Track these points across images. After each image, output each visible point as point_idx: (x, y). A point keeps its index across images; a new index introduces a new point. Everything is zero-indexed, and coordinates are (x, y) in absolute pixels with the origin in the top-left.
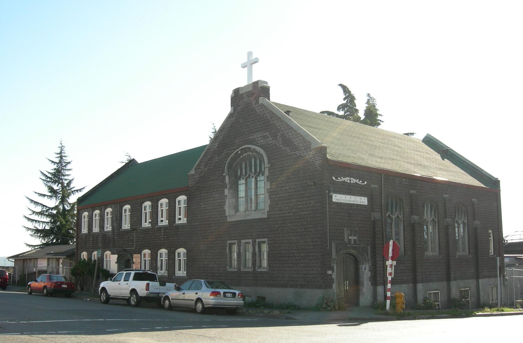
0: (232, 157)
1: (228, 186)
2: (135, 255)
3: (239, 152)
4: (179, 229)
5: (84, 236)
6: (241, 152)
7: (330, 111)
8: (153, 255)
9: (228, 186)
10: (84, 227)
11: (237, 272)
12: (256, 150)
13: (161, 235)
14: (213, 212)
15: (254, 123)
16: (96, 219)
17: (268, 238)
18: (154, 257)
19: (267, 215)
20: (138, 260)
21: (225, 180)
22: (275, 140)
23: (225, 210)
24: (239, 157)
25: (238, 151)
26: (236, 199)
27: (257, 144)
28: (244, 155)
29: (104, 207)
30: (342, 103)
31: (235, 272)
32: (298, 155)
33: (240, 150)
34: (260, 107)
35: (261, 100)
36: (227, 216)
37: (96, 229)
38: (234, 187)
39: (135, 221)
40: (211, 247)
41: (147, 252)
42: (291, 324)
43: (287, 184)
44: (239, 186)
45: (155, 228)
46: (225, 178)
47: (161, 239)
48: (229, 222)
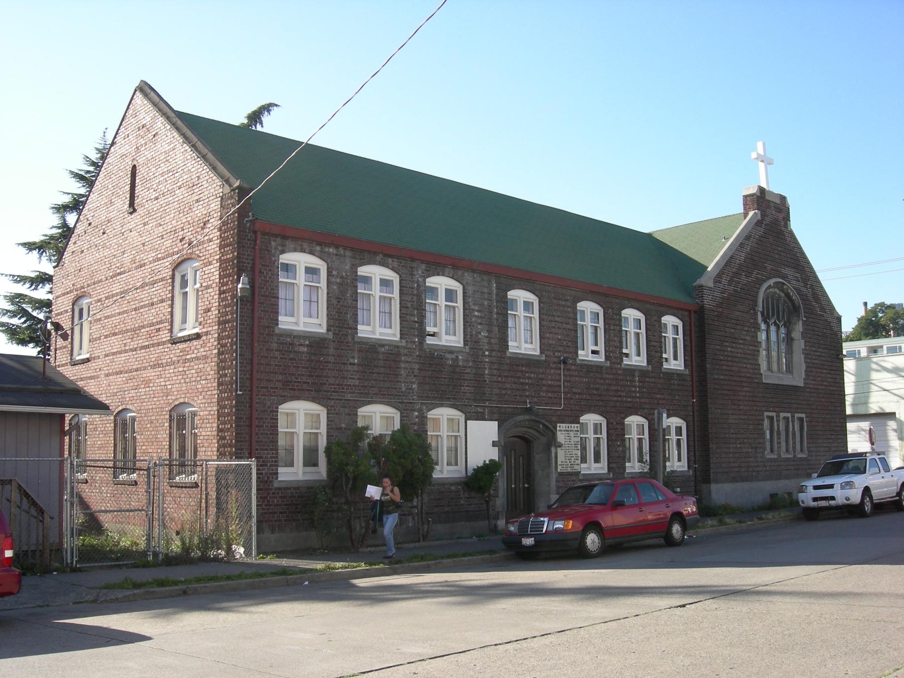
2: (561, 427)
4: (672, 379)
5: (307, 343)
7: (250, 112)
8: (617, 429)
11: (777, 459)
13: (635, 386)
14: (745, 363)
17: (806, 413)
18: (617, 434)
20: (572, 438)
29: (423, 266)
30: (259, 105)
31: (775, 458)
37: (636, 359)
39: (560, 340)
40: (744, 419)
41: (591, 419)
42: (218, 605)
45: (619, 369)
47: (634, 395)
48: (764, 383)
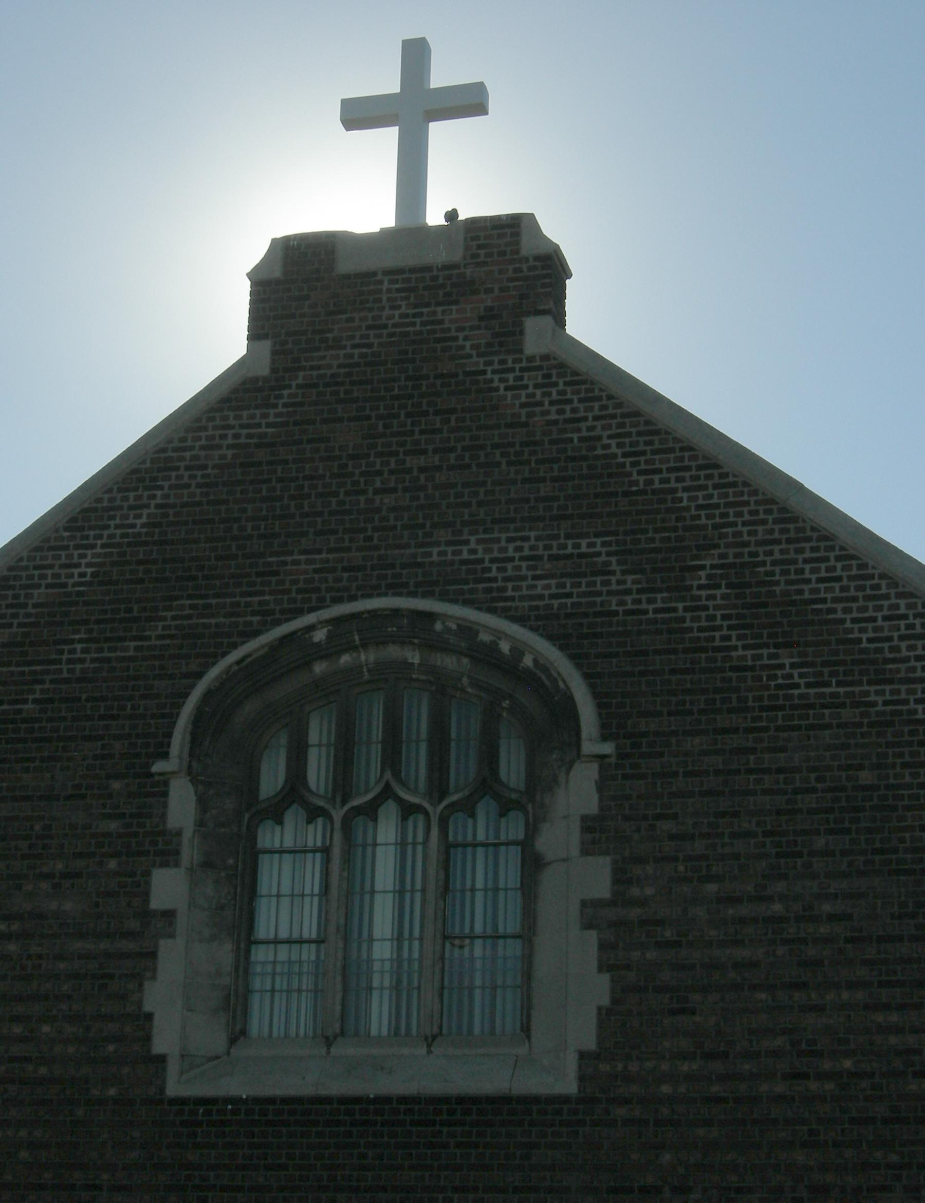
0: (244, 663)
1: (190, 851)
3: (320, 636)
6: (330, 637)
9: (190, 851)
10: (283, 1017)
12: (485, 637)
15: (468, 466)
16: (285, 983)
19: (581, 1079)
21: (165, 805)
22: (665, 595)
23: (149, 1017)
24: (307, 664)
25: (311, 628)
26: (242, 946)
27: (494, 600)
28: (345, 659)
32: (880, 708)
33: (336, 621)
34: (529, 379)
35: (533, 326)
36: (162, 1059)
38: (231, 861)
43: (781, 886)
44: (264, 860)
46: (165, 794)
48: (174, 1101)
